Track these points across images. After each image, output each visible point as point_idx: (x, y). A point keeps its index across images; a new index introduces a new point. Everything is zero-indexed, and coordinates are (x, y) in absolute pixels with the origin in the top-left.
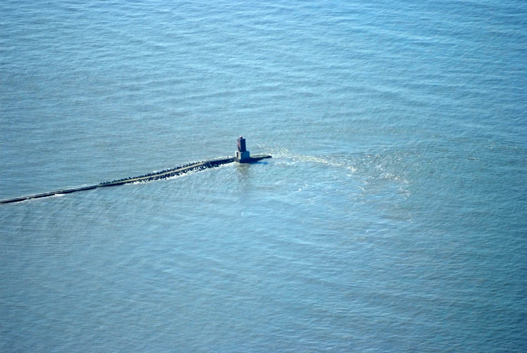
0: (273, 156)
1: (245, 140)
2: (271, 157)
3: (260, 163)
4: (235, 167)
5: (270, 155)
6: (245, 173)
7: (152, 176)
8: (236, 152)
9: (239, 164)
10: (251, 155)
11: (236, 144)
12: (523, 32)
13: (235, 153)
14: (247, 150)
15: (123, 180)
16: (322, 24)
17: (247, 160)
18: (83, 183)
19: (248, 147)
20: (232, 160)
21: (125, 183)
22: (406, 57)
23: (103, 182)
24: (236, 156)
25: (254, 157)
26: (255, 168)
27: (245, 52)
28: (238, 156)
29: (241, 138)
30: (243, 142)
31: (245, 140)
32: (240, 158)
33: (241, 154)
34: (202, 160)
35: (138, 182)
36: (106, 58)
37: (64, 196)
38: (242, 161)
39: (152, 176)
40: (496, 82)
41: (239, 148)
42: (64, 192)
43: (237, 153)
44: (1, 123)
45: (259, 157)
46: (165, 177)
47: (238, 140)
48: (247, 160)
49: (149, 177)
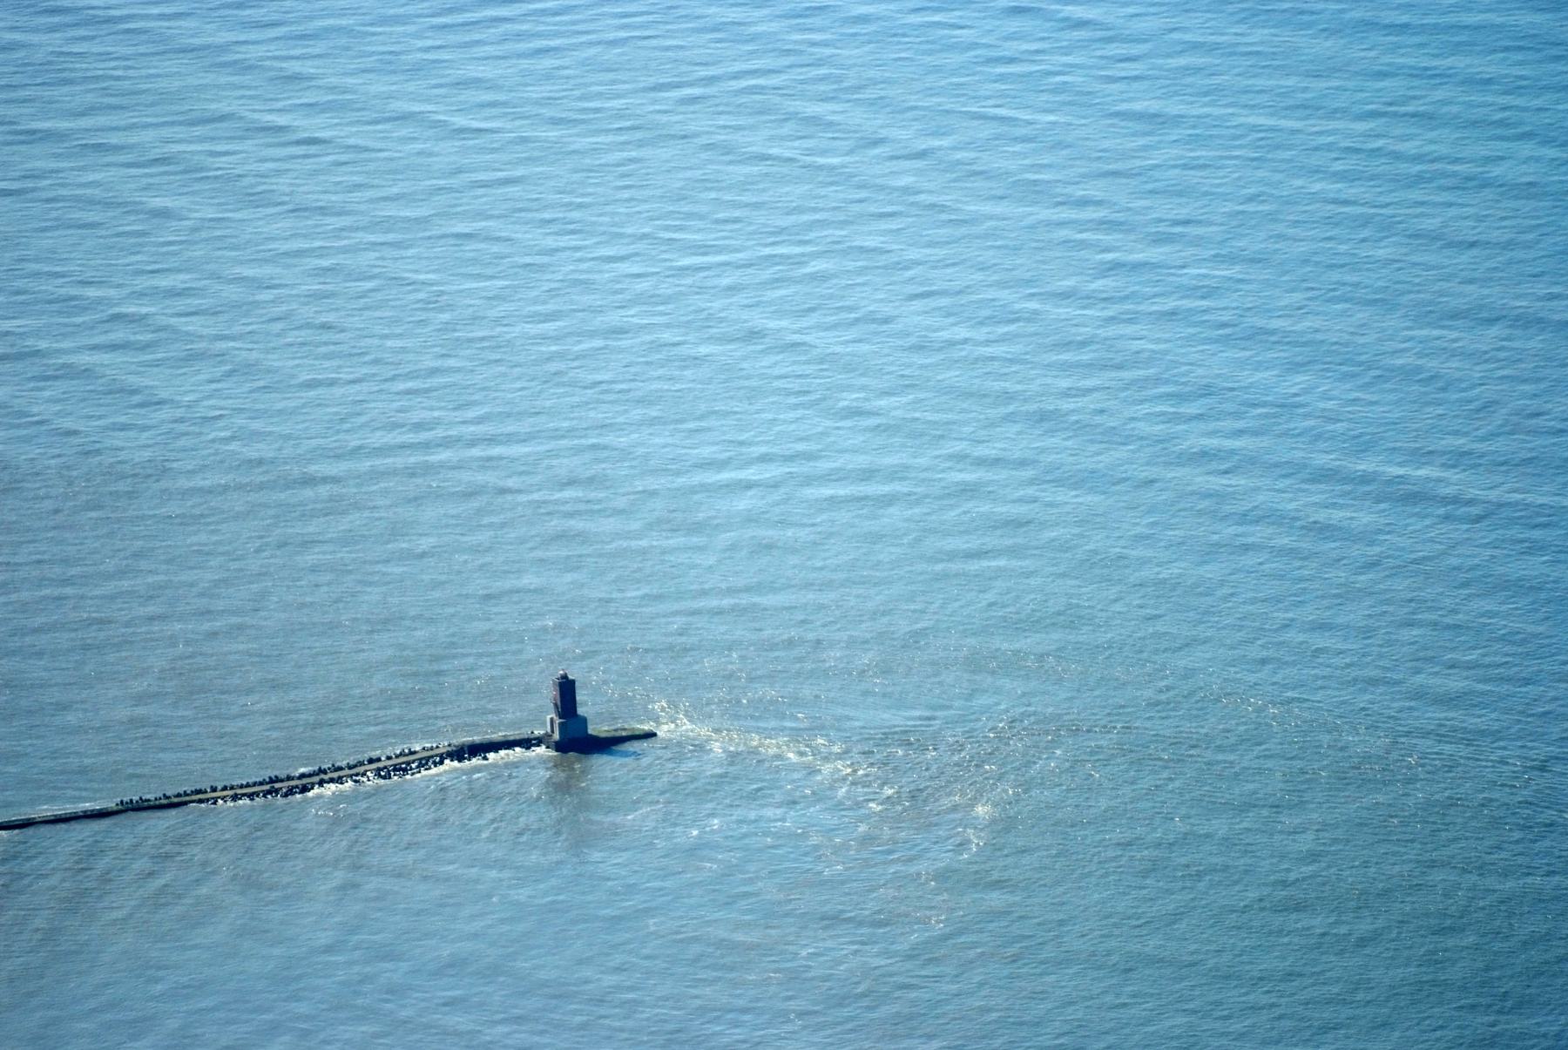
0: (663, 731)
1: (573, 682)
3: (626, 754)
4: (542, 761)
7: (277, 785)
9: (553, 753)
13: (546, 721)
14: (581, 711)
15: (186, 794)
17: (577, 741)
18: (85, 800)
19: (586, 705)
20: (539, 741)
22: (1419, 210)
25: (603, 735)
26: (602, 764)
29: (565, 677)
30: (567, 688)
31: (573, 682)
32: (556, 736)
33: (561, 725)
34: (444, 746)
36: (443, 455)
38: (561, 747)
39: (277, 785)
42: (459, 754)
45: (618, 734)
49: (267, 787)
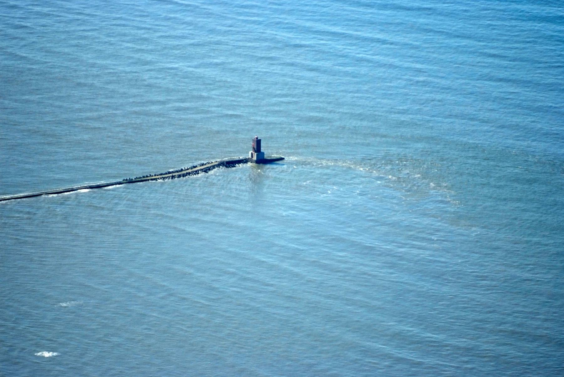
1: (260, 140)
2: (283, 159)
5: (283, 157)
6: (257, 181)
7: (174, 174)
8: (250, 153)
9: (254, 164)
10: (266, 157)
11: (251, 144)
13: (249, 154)
14: (262, 151)
16: (342, 91)
17: (262, 161)
20: (245, 161)
21: (148, 180)
23: (125, 179)
24: (250, 156)
28: (252, 156)
29: (257, 138)
30: (258, 142)
31: (260, 140)
32: (255, 158)
33: (257, 155)
37: (89, 192)
39: (174, 174)
40: (438, 90)
41: (254, 148)
43: (252, 154)
46: (184, 175)
48: (262, 161)
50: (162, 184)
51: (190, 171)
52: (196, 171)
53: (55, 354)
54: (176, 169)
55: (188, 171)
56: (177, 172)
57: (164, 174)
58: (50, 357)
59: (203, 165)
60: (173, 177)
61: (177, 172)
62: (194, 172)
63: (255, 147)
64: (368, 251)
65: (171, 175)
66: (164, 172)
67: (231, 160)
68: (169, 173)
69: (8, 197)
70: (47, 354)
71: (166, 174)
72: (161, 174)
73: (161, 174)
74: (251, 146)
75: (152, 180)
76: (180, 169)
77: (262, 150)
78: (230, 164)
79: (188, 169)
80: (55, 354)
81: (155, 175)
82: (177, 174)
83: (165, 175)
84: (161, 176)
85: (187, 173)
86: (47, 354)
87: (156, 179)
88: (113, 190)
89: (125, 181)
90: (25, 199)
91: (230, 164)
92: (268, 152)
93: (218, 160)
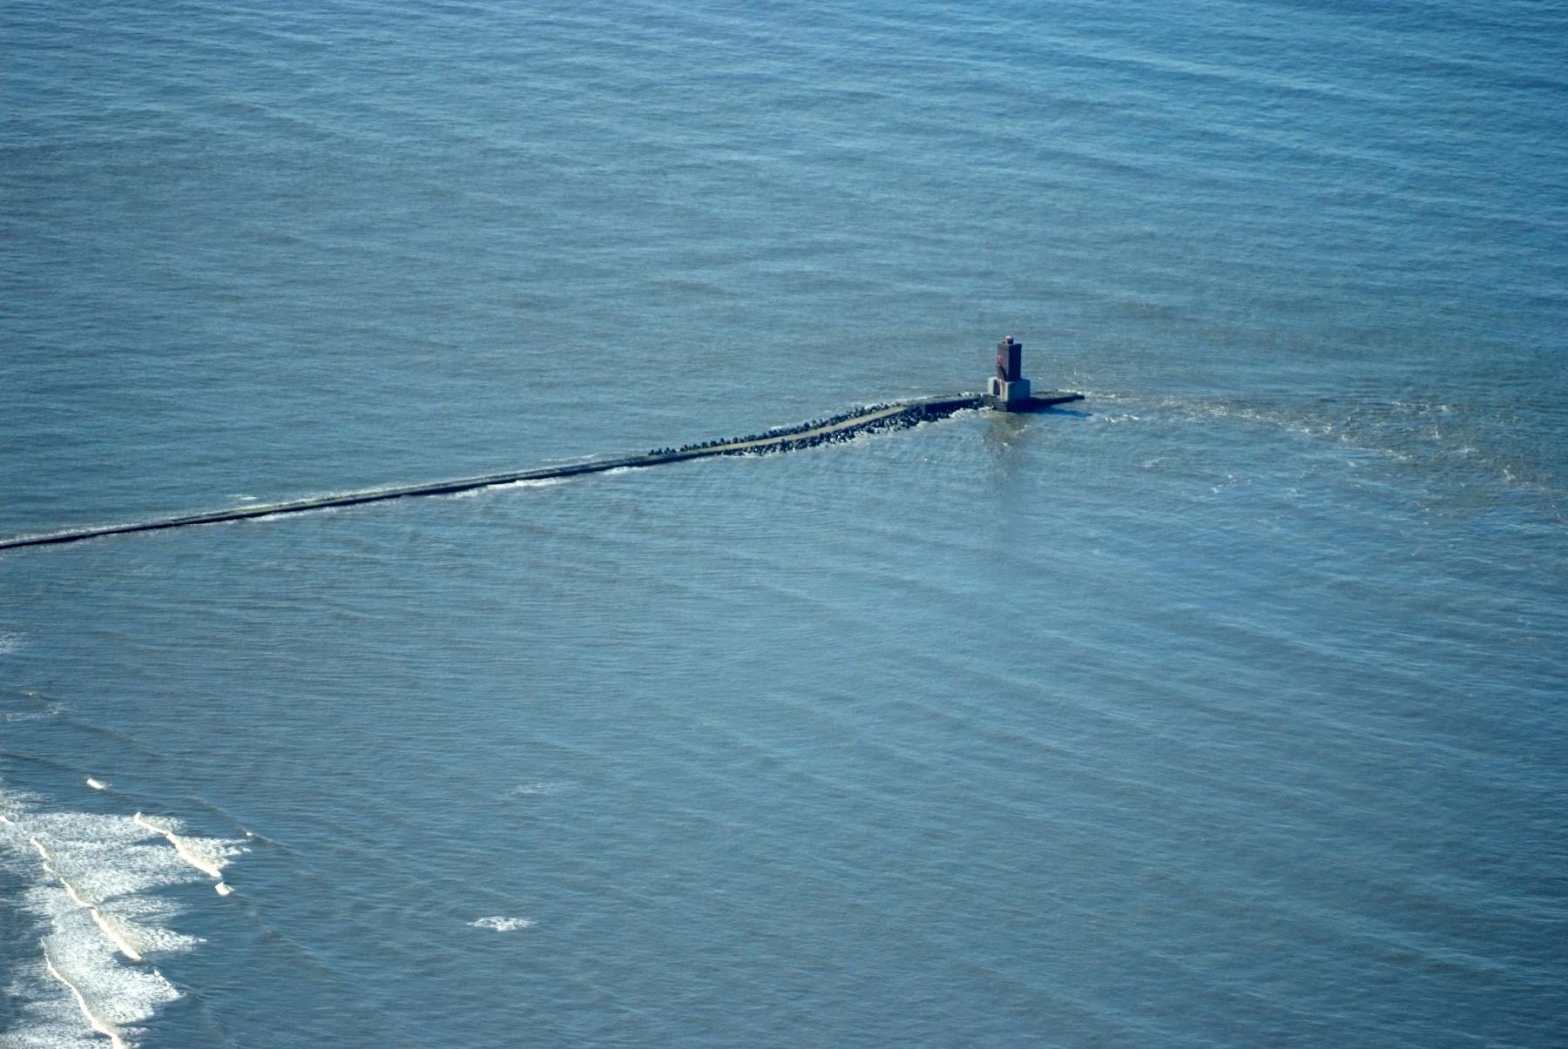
1: (1019, 346)
2: (1082, 397)
7: (787, 438)
8: (991, 380)
11: (995, 356)
12: (1560, 693)
20: (973, 404)
24: (991, 391)
26: (1037, 422)
27: (862, 829)
28: (997, 391)
29: (1011, 341)
30: (1014, 352)
31: (1019, 346)
32: (1004, 396)
33: (1011, 387)
35: (752, 456)
39: (787, 438)
41: (1001, 369)
42: (564, 473)
43: (996, 384)
44: (3, 679)
45: (1051, 396)
47: (1000, 347)
48: (1024, 404)
50: (753, 462)
51: (828, 429)
52: (846, 431)
53: (523, 923)
54: (788, 426)
55: (824, 430)
56: (795, 431)
57: (760, 438)
58: (509, 936)
59: (863, 413)
60: (785, 446)
61: (795, 431)
62: (840, 431)
63: (1006, 366)
64: (1270, 651)
65: (779, 440)
66: (741, 436)
67: (938, 401)
68: (774, 434)
69: (378, 490)
70: (502, 925)
71: (765, 437)
72: (752, 439)
73: (752, 439)
74: (994, 365)
75: (728, 452)
76: (802, 424)
77: (1025, 373)
78: (937, 410)
79: (823, 425)
80: (523, 923)
81: (736, 441)
82: (793, 437)
83: (764, 443)
84: (753, 444)
85: (822, 436)
86: (502, 925)
87: (740, 451)
88: (619, 479)
89: (654, 457)
90: (387, 503)
91: (937, 410)
92: (1040, 383)
93: (904, 400)
